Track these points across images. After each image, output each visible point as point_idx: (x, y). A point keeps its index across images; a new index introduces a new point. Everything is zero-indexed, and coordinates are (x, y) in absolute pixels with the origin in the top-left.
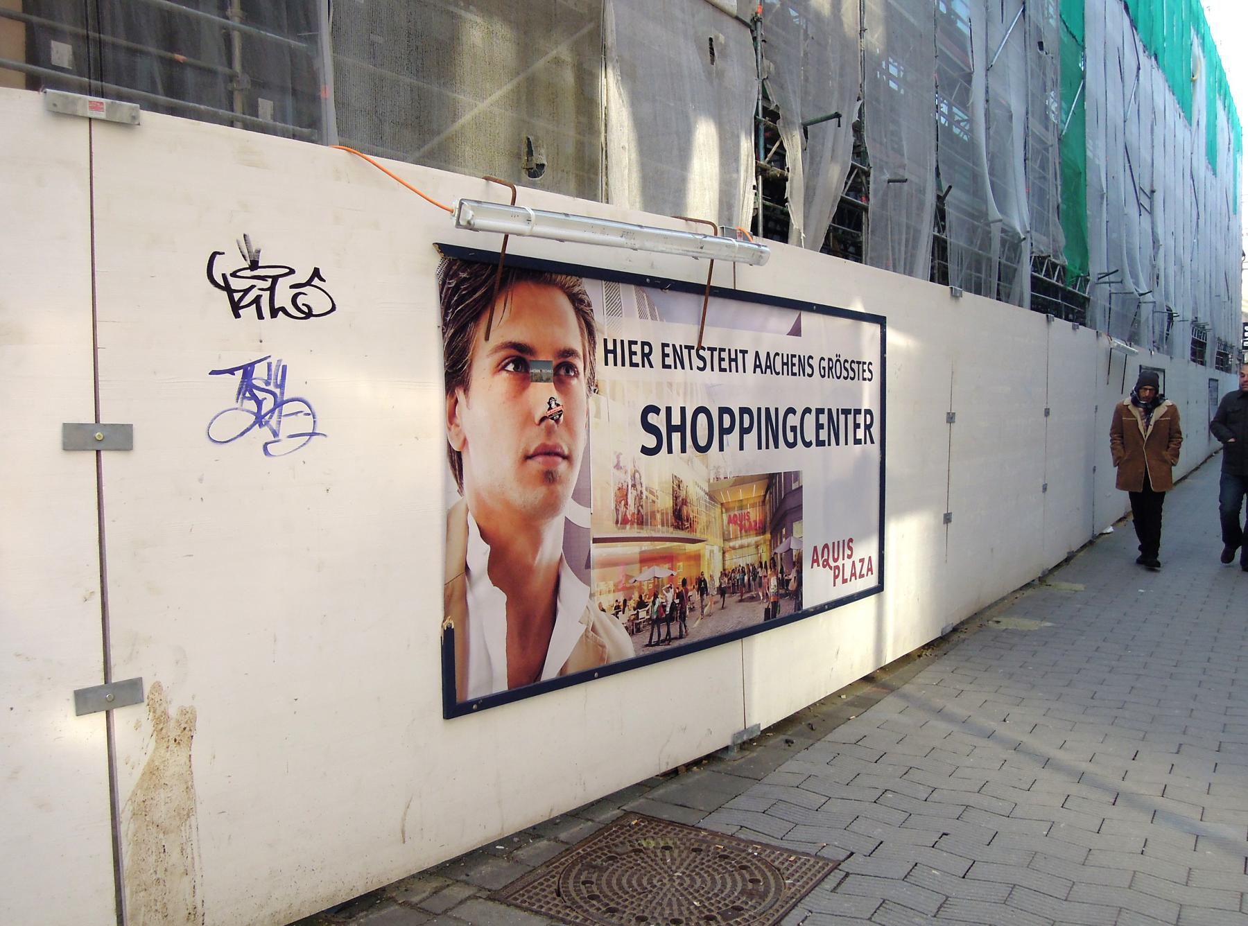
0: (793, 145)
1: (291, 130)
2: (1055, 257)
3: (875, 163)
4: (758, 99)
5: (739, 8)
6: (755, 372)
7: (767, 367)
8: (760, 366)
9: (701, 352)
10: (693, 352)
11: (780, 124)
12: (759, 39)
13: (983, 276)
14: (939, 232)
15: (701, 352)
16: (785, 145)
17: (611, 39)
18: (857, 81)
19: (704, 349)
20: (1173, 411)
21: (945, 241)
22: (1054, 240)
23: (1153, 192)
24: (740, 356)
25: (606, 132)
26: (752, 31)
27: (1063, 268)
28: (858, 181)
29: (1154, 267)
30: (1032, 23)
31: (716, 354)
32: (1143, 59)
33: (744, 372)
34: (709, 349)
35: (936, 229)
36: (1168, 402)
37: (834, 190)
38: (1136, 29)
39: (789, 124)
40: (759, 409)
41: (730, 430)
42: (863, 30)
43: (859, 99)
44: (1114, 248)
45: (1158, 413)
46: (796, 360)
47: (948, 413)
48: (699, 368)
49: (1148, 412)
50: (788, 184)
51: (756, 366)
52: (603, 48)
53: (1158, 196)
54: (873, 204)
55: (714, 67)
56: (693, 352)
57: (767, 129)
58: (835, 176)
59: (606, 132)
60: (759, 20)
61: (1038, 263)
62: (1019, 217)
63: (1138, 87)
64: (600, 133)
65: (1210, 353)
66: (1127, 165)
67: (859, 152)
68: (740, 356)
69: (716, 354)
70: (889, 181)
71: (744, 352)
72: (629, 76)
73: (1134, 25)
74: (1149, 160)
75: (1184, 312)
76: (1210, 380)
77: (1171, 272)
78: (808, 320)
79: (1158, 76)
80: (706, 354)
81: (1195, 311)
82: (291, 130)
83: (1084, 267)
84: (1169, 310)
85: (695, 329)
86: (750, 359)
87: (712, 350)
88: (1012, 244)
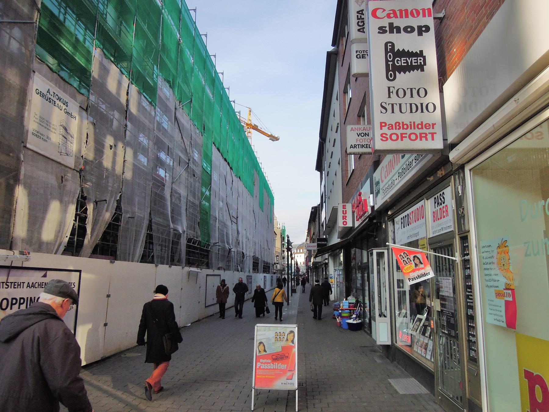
0: (90, 207)
1: (5, 18)
2: (197, 238)
3: (124, 211)
4: (79, 193)
5: (75, 166)
6: (27, 288)
7: (32, 286)
8: (29, 286)
9: (7, 284)
10: (4, 284)
11: (86, 201)
12: (82, 176)
13: (167, 245)
14: (149, 232)
15: (7, 284)
16: (88, 207)
17: (22, 177)
18: (120, 187)
19: (8, 283)
20: (228, 287)
21: (152, 235)
22: (196, 233)
23: (237, 217)
24: (22, 284)
25: (16, 204)
26: (80, 173)
27: (200, 241)
28: (117, 218)
29: (237, 240)
30: (191, 169)
31: (13, 284)
32: (235, 178)
33: (23, 288)
34: (10, 283)
35: (149, 231)
36: (227, 286)
37: (107, 220)
38: (232, 170)
39: (90, 201)
40: (27, 298)
41: (15, 304)
42: (123, 173)
43: (120, 193)
44: (221, 234)
45: (225, 287)
46: (44, 284)
47: (107, 295)
48: (6, 288)
49: (223, 288)
50: (87, 219)
51: (27, 286)
52: (19, 180)
53: (240, 219)
54: (122, 224)
55: (62, 184)
56: (4, 284)
57: (81, 202)
58: (107, 216)
59: (16, 204)
60: (82, 170)
61: (189, 240)
62: (182, 227)
63: (232, 186)
64: (14, 205)
65: (261, 266)
66: (227, 209)
67: (118, 208)
68: (22, 284)
69: (13, 284)
70: (129, 217)
71: (23, 283)
72: (28, 187)
73: (231, 168)
74: (237, 208)
75: (249, 253)
76: (247, 276)
77: (244, 242)
78: (49, 273)
79: (240, 183)
80: (9, 284)
81: (255, 253)
82: (5, 18)
83: (208, 241)
84: (243, 253)
85: (6, 278)
86: (26, 285)
87: (11, 283)
88: (178, 236)
